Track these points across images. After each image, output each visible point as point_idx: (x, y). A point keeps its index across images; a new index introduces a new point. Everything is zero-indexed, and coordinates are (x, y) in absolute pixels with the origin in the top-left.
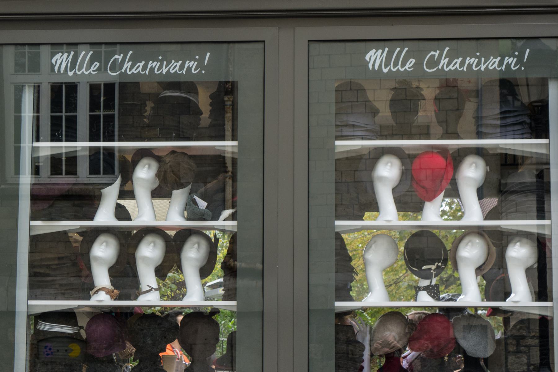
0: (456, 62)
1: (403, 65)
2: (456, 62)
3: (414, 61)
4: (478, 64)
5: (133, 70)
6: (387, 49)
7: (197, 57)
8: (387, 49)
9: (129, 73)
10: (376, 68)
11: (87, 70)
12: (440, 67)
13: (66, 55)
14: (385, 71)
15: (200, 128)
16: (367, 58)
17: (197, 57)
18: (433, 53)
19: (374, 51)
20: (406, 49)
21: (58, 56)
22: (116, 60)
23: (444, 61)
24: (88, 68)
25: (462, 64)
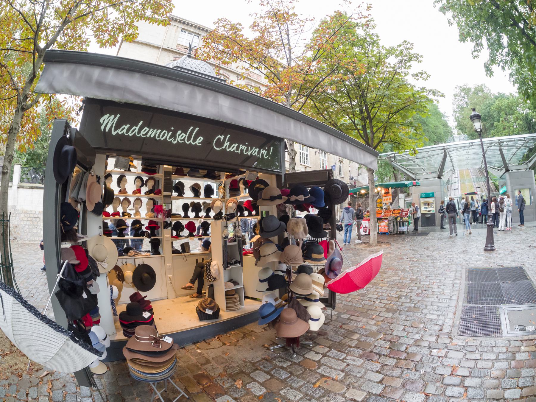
0: (124, 128)
1: (194, 140)
2: (124, 128)
3: (202, 139)
4: (247, 150)
5: (230, 149)
6: (118, 115)
7: (172, 128)
8: (118, 115)
9: (228, 150)
10: (107, 130)
11: (194, 142)
12: (224, 147)
13: (113, 116)
14: (114, 133)
15: (317, 373)
16: (101, 121)
17: (172, 128)
18: (219, 136)
19: (108, 115)
20: (197, 129)
21: (106, 116)
22: (219, 139)
23: (227, 144)
24: (194, 141)
25: (238, 148)
